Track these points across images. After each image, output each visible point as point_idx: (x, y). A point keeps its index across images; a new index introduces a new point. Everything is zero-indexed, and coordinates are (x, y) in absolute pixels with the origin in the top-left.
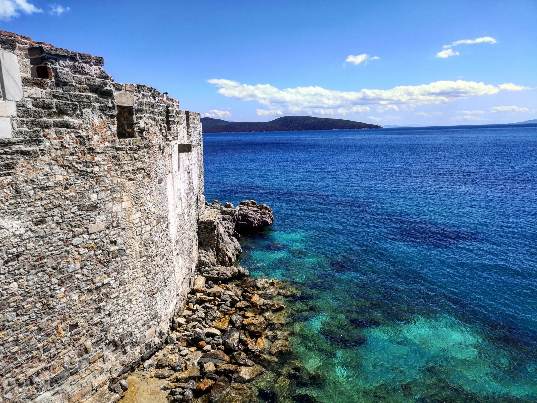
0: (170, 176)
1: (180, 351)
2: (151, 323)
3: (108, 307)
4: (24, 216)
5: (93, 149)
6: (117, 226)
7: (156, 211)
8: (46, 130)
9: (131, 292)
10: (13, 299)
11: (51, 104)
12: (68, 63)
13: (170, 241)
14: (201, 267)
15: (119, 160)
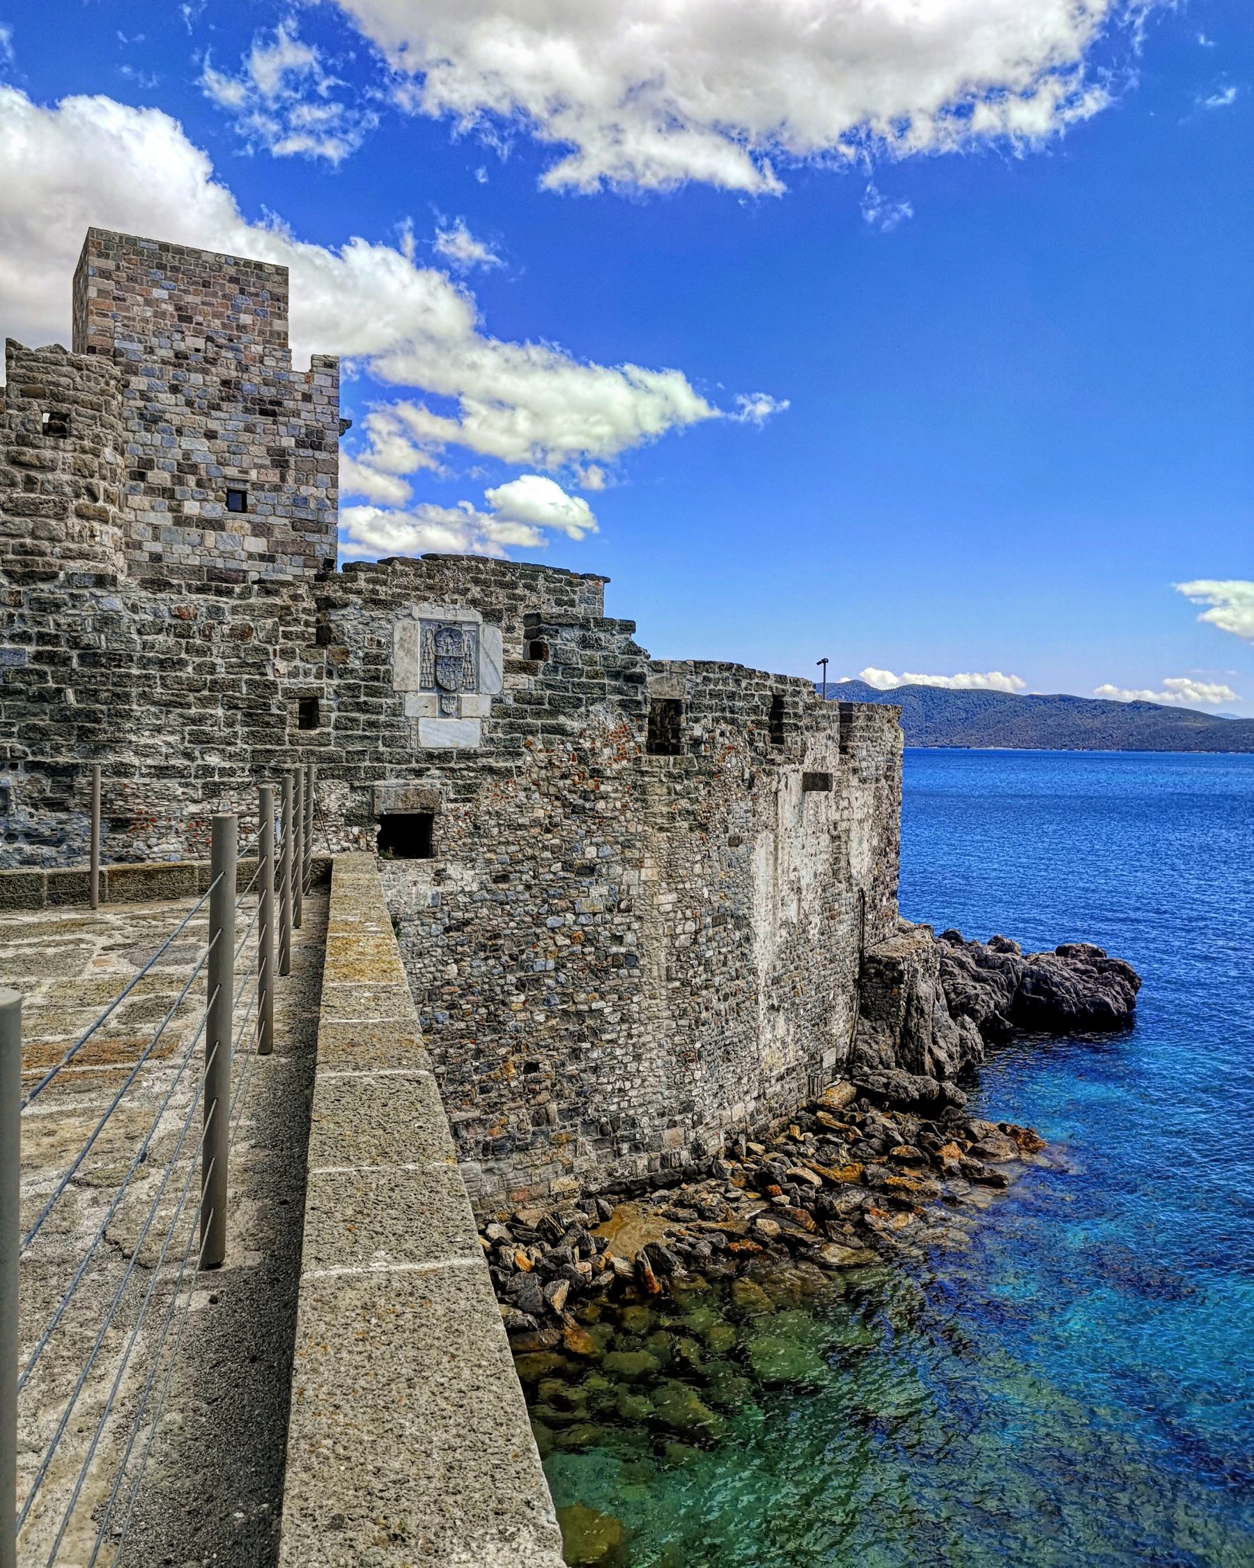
0: (765, 837)
1: (727, 1191)
2: (678, 1118)
3: (595, 1055)
4: (480, 863)
5: (599, 771)
6: (628, 910)
7: (714, 898)
8: (530, 738)
9: (642, 1040)
10: (446, 989)
11: (542, 698)
12: (577, 633)
13: (753, 971)
14: (849, 1065)
15: (644, 793)
